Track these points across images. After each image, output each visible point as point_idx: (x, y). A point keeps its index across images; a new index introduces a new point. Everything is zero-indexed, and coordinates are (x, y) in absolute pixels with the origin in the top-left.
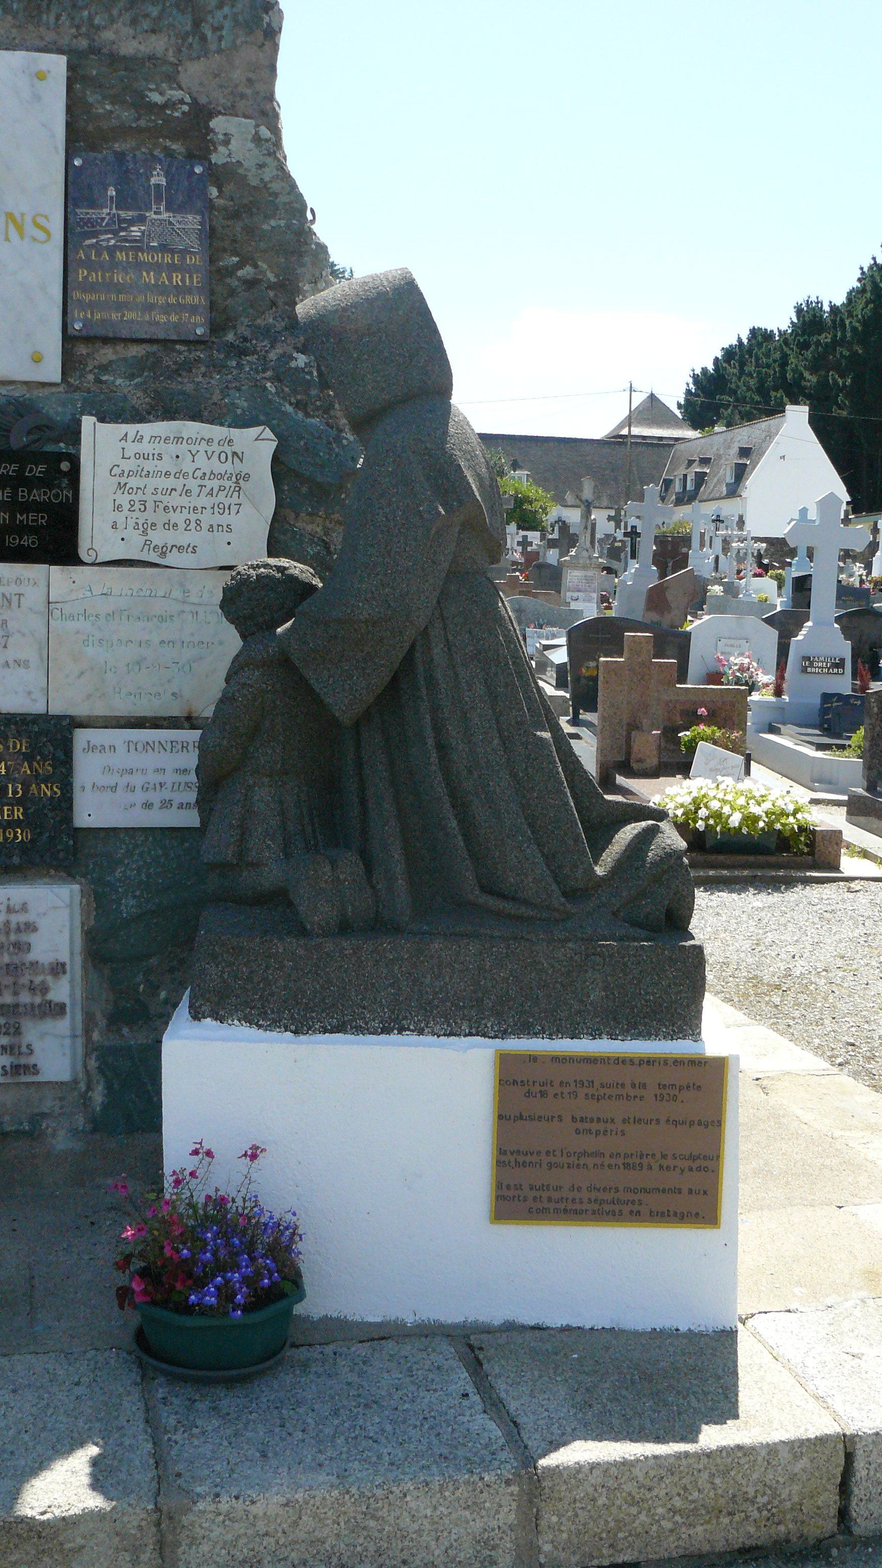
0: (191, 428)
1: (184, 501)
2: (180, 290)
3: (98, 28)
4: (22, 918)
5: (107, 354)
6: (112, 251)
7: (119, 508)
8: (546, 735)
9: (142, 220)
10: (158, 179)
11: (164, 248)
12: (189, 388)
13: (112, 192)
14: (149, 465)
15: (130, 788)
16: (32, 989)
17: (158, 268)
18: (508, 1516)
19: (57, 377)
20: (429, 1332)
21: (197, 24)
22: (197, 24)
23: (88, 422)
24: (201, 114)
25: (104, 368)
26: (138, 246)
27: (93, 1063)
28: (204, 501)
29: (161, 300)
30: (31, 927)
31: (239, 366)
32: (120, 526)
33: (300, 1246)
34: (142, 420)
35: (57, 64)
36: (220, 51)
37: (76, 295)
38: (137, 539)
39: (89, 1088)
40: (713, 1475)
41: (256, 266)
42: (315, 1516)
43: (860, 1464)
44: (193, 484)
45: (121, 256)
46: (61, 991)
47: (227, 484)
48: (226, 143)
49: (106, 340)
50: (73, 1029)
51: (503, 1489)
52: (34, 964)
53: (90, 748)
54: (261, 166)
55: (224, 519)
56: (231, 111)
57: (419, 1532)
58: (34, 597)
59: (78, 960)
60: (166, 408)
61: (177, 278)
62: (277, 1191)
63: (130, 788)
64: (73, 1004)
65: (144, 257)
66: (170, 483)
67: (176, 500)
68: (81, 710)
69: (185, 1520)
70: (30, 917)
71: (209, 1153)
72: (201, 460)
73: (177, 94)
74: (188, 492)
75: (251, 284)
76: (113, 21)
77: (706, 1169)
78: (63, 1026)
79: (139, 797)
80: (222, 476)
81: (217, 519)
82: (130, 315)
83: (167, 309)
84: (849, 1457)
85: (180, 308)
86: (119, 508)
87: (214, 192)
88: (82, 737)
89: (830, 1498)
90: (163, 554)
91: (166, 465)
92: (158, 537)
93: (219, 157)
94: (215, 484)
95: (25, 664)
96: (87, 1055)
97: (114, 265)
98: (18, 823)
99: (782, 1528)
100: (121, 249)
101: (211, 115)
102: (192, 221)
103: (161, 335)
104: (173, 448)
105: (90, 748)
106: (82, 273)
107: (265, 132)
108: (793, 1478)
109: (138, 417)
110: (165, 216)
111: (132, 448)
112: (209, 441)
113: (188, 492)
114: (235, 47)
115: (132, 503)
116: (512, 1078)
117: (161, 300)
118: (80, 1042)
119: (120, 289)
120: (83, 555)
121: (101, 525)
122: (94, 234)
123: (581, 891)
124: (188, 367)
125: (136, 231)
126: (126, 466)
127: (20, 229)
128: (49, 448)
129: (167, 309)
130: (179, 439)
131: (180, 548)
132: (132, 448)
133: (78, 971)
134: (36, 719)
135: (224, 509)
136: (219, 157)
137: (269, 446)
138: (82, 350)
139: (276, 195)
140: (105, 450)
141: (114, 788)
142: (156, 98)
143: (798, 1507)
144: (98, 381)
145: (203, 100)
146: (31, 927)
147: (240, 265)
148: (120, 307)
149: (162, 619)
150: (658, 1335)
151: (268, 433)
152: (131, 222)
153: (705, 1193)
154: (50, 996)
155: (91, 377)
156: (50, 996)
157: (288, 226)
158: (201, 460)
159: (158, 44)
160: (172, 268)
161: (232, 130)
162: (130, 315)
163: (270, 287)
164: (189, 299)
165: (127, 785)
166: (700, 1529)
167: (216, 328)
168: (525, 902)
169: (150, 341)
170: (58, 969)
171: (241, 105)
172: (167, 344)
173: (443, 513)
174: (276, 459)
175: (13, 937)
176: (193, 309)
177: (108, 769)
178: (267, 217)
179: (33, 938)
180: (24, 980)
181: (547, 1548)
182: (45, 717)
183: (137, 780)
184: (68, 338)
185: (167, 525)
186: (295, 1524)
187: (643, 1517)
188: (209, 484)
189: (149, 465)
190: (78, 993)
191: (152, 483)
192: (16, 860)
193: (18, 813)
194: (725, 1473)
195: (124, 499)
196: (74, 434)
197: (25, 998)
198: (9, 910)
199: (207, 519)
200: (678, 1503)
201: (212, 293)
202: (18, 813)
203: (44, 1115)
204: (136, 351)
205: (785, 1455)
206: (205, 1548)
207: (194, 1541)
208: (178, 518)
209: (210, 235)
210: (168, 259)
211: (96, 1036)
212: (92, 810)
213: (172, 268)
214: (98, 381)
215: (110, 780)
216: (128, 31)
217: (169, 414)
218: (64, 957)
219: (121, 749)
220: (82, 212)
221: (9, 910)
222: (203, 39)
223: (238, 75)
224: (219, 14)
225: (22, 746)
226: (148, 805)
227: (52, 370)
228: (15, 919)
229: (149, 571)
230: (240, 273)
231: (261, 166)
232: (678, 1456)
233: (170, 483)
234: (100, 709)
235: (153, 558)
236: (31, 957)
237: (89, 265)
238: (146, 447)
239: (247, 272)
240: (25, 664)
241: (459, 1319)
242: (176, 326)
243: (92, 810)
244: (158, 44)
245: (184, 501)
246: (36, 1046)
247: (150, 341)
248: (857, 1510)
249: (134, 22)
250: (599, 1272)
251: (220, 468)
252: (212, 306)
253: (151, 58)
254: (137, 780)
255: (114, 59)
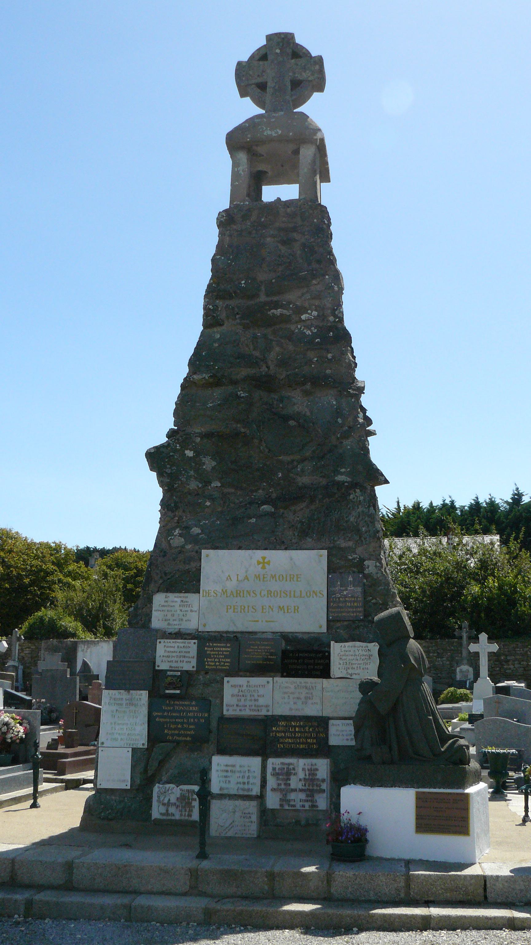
0: (358, 644)
1: (356, 662)
2: (356, 607)
3: (336, 541)
4: (315, 767)
5: (338, 624)
6: (339, 598)
7: (340, 664)
8: (431, 717)
9: (347, 590)
10: (350, 579)
11: (352, 597)
12: (358, 633)
13: (339, 583)
14: (347, 653)
15: (343, 735)
16: (317, 786)
17: (350, 602)
18: (402, 884)
19: (325, 631)
20: (400, 860)
21: (360, 537)
22: (360, 537)
23: (332, 643)
24: (362, 560)
25: (338, 628)
26: (346, 596)
27: (332, 807)
28: (362, 662)
29: (352, 610)
30: (317, 770)
31: (372, 626)
32: (341, 668)
33: (368, 834)
34: (347, 642)
35: (325, 552)
36: (366, 544)
37: (330, 610)
38: (345, 672)
39: (331, 812)
40: (451, 881)
41: (376, 599)
42: (360, 878)
43: (488, 883)
44: (358, 658)
45: (341, 599)
46: (324, 786)
47: (367, 657)
48: (368, 568)
49: (338, 621)
50: (327, 796)
51: (401, 877)
52: (318, 779)
53: (333, 725)
54: (377, 573)
55: (367, 667)
56: (369, 559)
57: (383, 885)
58: (319, 687)
59: (329, 779)
60: (353, 639)
61: (355, 604)
62: (363, 822)
63: (343, 735)
64: (327, 789)
65: (347, 599)
66: (353, 657)
67: (354, 662)
68: (331, 715)
69: (333, 876)
70: (317, 767)
71: (348, 813)
72: (360, 652)
73: (355, 556)
74: (357, 660)
75: (374, 604)
76: (339, 538)
77: (464, 821)
78: (325, 795)
79: (345, 737)
80: (365, 656)
81: (364, 667)
82: (343, 614)
83: (353, 612)
84: (485, 881)
85: (356, 612)
86: (340, 664)
87: (365, 581)
88: (331, 722)
89: (481, 891)
90: (351, 676)
91: (351, 653)
92: (350, 671)
93: (366, 572)
94: (364, 657)
95: (317, 703)
96: (331, 804)
97: (339, 602)
98: (315, 743)
99: (469, 897)
100: (341, 597)
101: (364, 560)
102: (359, 589)
103: (351, 619)
104: (353, 649)
105: (333, 725)
106: (332, 604)
107: (378, 564)
108: (471, 884)
109: (347, 641)
110: (352, 588)
111: (343, 649)
112: (362, 647)
113: (357, 660)
114: (370, 543)
115: (343, 663)
116: (419, 798)
117: (352, 610)
118: (329, 800)
119: (341, 607)
120: (331, 676)
121: (336, 669)
122: (335, 594)
123: (437, 755)
124: (358, 627)
125: (345, 593)
126: (342, 653)
127: (316, 595)
128: (323, 649)
129: (353, 612)
130: (355, 646)
131: (355, 674)
132: (343, 649)
133: (329, 781)
134: (319, 717)
135: (366, 664)
136: (366, 572)
137: (377, 648)
138: (332, 623)
139: (381, 580)
140: (337, 650)
141: (339, 735)
142: (350, 557)
143: (473, 892)
144: (336, 631)
145: (362, 557)
146: (317, 770)
147: (372, 599)
148: (341, 612)
149: (351, 692)
150: (507, 909)
151: (377, 644)
152: (344, 590)
153: (263, 696)
154: (322, 787)
155: (334, 630)
156: (322, 787)
157: (384, 588)
158: (360, 652)
159: (351, 544)
160: (354, 602)
161: (370, 564)
162: (343, 614)
163: (381, 604)
164: (359, 610)
165: (341, 734)
166: (448, 894)
167: (366, 616)
168: (425, 757)
169: (348, 621)
170: (323, 781)
171: (372, 557)
172: (353, 622)
173: (167, 691)
174: (379, 651)
175: (312, 772)
176: (360, 612)
177: (337, 730)
178: (379, 587)
179: (318, 773)
180: (315, 783)
181: (412, 893)
182: (322, 717)
183: (345, 733)
184: (328, 621)
185: (353, 668)
186: (356, 879)
187: (434, 889)
188: (362, 658)
189: (347, 653)
190: (329, 786)
191: (348, 658)
192: (314, 753)
193: (315, 741)
194: (454, 881)
195: (341, 662)
196: (329, 646)
197: (315, 788)
198: (312, 765)
199: (362, 666)
200: (442, 886)
201: (365, 607)
202: (315, 741)
203: (320, 820)
204: (345, 623)
205: (469, 878)
206: (337, 883)
207: (335, 881)
208: (355, 666)
209: (365, 593)
210: (353, 599)
211: (333, 800)
212: (333, 741)
213: (354, 602)
214: (336, 631)
215: (338, 733)
216: (343, 541)
217: (353, 640)
218: (325, 777)
219: (341, 725)
220: (332, 589)
221: (312, 765)
222: (362, 541)
223: (371, 550)
224: (366, 535)
225: (316, 724)
226: (347, 740)
227: (324, 629)
228: (313, 767)
229: (348, 680)
230: (372, 601)
231: (377, 573)
232: (442, 875)
233: (353, 657)
234: (335, 715)
235: (349, 676)
236: (317, 777)
237: (334, 602)
238: (347, 649)
239: (374, 601)
240: (317, 703)
241: (408, 858)
242: (356, 616)
243: (333, 741)
244: (351, 544)
245: (356, 662)
246: (318, 800)
247: (348, 621)
248: (488, 895)
249: (344, 539)
250: (440, 845)
251: (365, 653)
252: (365, 611)
253: (349, 547)
254: (345, 733)
255: (340, 549)
